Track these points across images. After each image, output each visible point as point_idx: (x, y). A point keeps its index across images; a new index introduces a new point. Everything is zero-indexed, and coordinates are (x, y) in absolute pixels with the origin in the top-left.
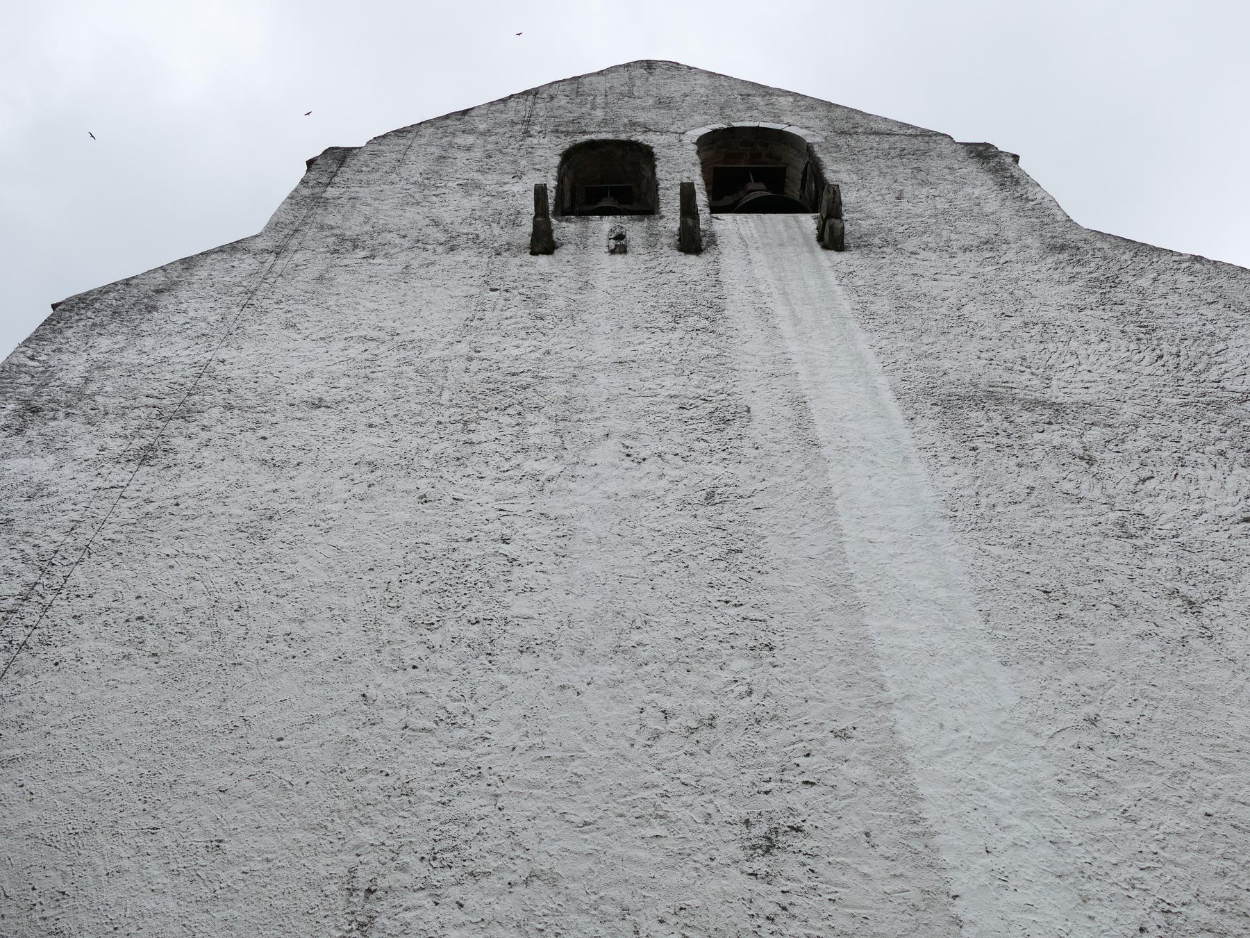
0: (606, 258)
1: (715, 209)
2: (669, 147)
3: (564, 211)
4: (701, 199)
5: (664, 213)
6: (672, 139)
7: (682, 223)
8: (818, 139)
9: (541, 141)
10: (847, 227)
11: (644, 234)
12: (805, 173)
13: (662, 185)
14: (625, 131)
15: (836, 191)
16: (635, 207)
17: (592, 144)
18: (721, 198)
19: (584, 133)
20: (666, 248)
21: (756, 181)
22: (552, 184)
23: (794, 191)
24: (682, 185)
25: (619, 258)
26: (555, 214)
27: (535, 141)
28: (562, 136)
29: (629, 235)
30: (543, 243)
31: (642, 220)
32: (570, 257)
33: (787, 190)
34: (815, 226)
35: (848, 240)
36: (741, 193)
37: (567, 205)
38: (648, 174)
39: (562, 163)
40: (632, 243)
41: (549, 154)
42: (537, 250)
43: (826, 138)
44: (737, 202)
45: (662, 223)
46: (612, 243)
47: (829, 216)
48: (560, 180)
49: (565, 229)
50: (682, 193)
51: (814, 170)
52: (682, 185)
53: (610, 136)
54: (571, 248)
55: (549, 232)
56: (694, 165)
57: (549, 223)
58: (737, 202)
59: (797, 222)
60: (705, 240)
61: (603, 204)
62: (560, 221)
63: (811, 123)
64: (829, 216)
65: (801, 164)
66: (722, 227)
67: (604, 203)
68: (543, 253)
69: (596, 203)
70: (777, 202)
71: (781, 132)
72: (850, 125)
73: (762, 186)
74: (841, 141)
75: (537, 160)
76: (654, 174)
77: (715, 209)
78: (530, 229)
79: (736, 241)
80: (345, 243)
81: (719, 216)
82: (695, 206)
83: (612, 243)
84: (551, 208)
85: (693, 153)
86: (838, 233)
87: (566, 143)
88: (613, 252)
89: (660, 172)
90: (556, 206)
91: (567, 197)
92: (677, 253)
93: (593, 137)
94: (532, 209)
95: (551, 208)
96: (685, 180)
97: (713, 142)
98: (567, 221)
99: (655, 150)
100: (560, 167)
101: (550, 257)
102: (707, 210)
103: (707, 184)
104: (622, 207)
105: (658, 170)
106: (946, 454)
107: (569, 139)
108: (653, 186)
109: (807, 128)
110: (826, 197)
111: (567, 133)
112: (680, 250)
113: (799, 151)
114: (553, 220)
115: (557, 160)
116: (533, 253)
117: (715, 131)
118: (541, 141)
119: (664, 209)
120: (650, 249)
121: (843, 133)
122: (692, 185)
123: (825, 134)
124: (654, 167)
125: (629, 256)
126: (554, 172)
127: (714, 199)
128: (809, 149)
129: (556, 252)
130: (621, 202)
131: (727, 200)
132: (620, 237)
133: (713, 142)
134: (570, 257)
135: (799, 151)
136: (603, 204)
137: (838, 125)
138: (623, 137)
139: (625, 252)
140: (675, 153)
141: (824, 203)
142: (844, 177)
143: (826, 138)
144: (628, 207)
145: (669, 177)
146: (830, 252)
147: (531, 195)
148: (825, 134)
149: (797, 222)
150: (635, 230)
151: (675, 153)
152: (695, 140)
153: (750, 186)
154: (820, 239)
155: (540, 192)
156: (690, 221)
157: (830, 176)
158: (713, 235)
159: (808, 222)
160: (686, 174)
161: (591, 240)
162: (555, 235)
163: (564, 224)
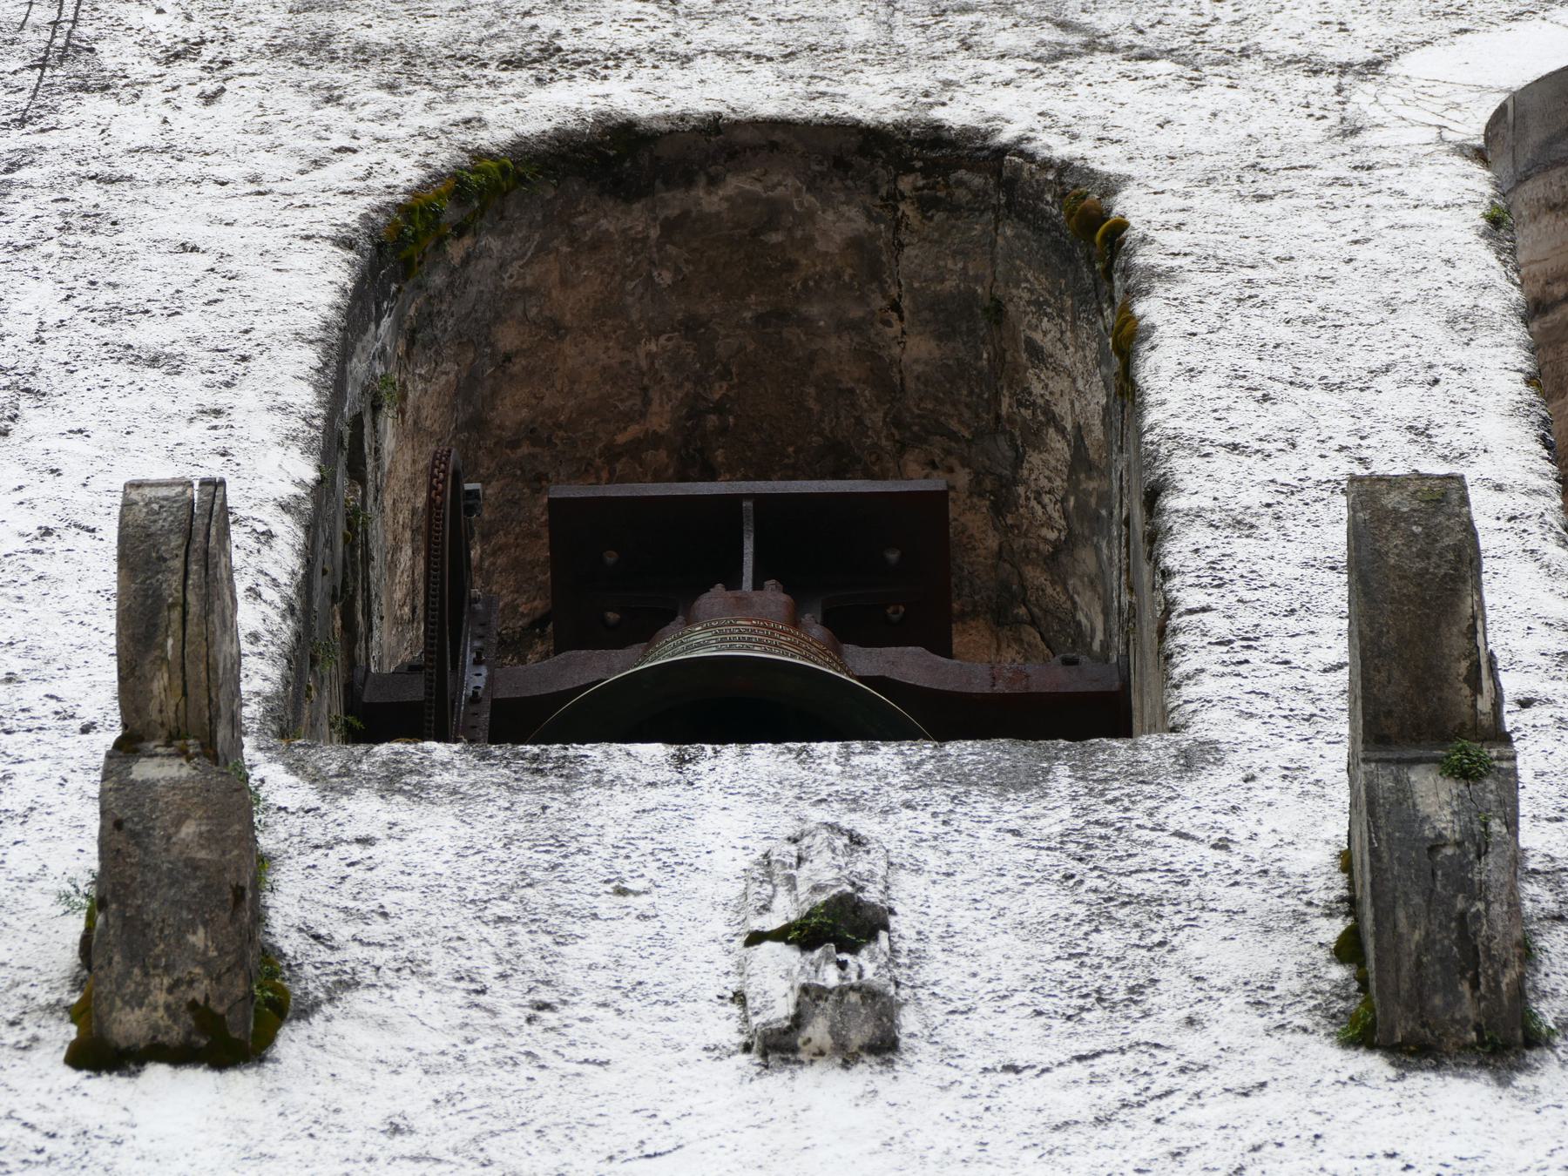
0: (734, 1085)
2: (1255, 178)
3: (371, 706)
5: (1211, 724)
6: (1277, 112)
9: (191, 121)
11: (1046, 901)
13: (1194, 487)
14: (887, 54)
16: (974, 665)
17: (613, 158)
19: (548, 59)
20: (1232, 1021)
22: (268, 475)
24: (1369, 498)
25: (825, 1093)
26: (289, 724)
27: (136, 124)
28: (362, 85)
29: (914, 906)
30: (182, 970)
31: (1033, 781)
32: (410, 1094)
37: (392, 643)
38: (1078, 396)
39: (361, 305)
40: (943, 971)
41: (247, 229)
42: (129, 1024)
45: (1197, 801)
46: (778, 977)
48: (343, 446)
49: (371, 850)
50: (1367, 566)
52: (1369, 498)
53: (761, 94)
54: (424, 1013)
55: (237, 889)
56: (1462, 323)
57: (236, 805)
61: (701, 640)
62: (334, 785)
67: (709, 636)
68: (180, 1056)
69: (644, 629)
75: (148, 278)
76: (1127, 395)
78: (75, 854)
80: (1553, 859)
82: (1480, 669)
83: (778, 977)
84: (260, 677)
85: (1461, 233)
87: (398, 144)
88: (777, 1047)
89: (1184, 382)
90: (302, 658)
91: (397, 578)
93: (631, 96)
94: (95, 687)
95: (260, 677)
96: (1394, 458)
98: (391, 782)
99: (1131, 206)
100: (344, 339)
101: (240, 1084)
104: (864, 663)
105: (1158, 370)
107: (419, 111)
108: (1124, 498)
111: (408, 65)
112: (1361, 1033)
114: (272, 777)
115: (319, 283)
116: (97, 1053)
118: (191, 121)
119: (1204, 687)
120: (1098, 1030)
122: (1446, 497)
124: (1127, 342)
125: (913, 1081)
126: (290, 382)
129: (291, 1043)
130: (847, 628)
132: (843, 924)
134: (410, 1094)
136: (701, 640)
138: (872, 98)
139: (885, 1047)
140: (1297, 226)
144: (910, 664)
145: (1250, 421)
147: (92, 575)
150: (959, 847)
151: (1297, 226)
152: (1472, 126)
155: (169, 557)
156: (1434, 797)
160: (1399, 401)
161: (594, 945)
162: (289, 908)
163: (366, 810)
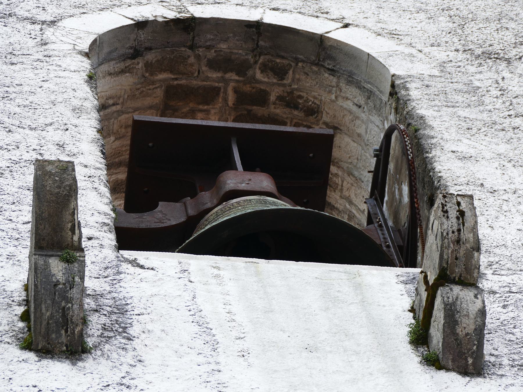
1: (128, 239)
4: (95, 207)
7: (36, 270)
8: (421, 68)
10: (494, 309)
12: (383, 154)
15: (464, 214)
18: (151, 207)
21: (248, 167)
23: (351, 202)
24: (42, 168)
33: (333, 197)
34: (407, 303)
35: (493, 346)
36: (206, 198)
43: (442, 65)
44: (193, 222)
47: (444, 278)
51: (406, 154)
52: (42, 168)
56: (77, 110)
58: (193, 222)
59: (358, 287)
60: (96, 322)
63: (402, 25)
64: (444, 278)
65: (372, 129)
66: (147, 289)
70: (306, 234)
71: (320, 42)
72: (509, 37)
73: (264, 181)
74: (485, 77)
77: (128, 239)
79: (187, 330)
81: (141, 256)
82: (75, 227)
86: (466, 325)
92: (15, 352)
96: (51, 154)
97: (136, 53)
102: (110, 239)
103: (111, 166)
106: (475, 128)
109: (393, 35)
110: (437, 225)
112: (27, 346)
113: (370, 95)
117: (141, 25)
121: (490, 56)
122: (67, 168)
123: (440, 55)
127: (131, 206)
128: (396, 91)
131: (168, 214)
133: (136, 53)
135: (370, 95)
137: (475, 34)
141: (432, 242)
142: (488, 173)
143: (442, 65)
146: (442, 375)
148: (440, 55)
149: (358, 287)
152: (85, 45)
153: (234, 179)
154: (420, 337)
156: (57, 268)
157: (450, 168)
158: (121, 309)
159: (387, 292)
160: (54, 135)
